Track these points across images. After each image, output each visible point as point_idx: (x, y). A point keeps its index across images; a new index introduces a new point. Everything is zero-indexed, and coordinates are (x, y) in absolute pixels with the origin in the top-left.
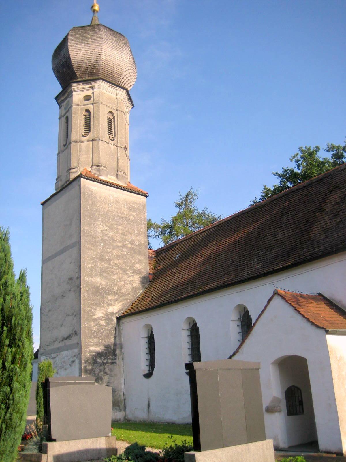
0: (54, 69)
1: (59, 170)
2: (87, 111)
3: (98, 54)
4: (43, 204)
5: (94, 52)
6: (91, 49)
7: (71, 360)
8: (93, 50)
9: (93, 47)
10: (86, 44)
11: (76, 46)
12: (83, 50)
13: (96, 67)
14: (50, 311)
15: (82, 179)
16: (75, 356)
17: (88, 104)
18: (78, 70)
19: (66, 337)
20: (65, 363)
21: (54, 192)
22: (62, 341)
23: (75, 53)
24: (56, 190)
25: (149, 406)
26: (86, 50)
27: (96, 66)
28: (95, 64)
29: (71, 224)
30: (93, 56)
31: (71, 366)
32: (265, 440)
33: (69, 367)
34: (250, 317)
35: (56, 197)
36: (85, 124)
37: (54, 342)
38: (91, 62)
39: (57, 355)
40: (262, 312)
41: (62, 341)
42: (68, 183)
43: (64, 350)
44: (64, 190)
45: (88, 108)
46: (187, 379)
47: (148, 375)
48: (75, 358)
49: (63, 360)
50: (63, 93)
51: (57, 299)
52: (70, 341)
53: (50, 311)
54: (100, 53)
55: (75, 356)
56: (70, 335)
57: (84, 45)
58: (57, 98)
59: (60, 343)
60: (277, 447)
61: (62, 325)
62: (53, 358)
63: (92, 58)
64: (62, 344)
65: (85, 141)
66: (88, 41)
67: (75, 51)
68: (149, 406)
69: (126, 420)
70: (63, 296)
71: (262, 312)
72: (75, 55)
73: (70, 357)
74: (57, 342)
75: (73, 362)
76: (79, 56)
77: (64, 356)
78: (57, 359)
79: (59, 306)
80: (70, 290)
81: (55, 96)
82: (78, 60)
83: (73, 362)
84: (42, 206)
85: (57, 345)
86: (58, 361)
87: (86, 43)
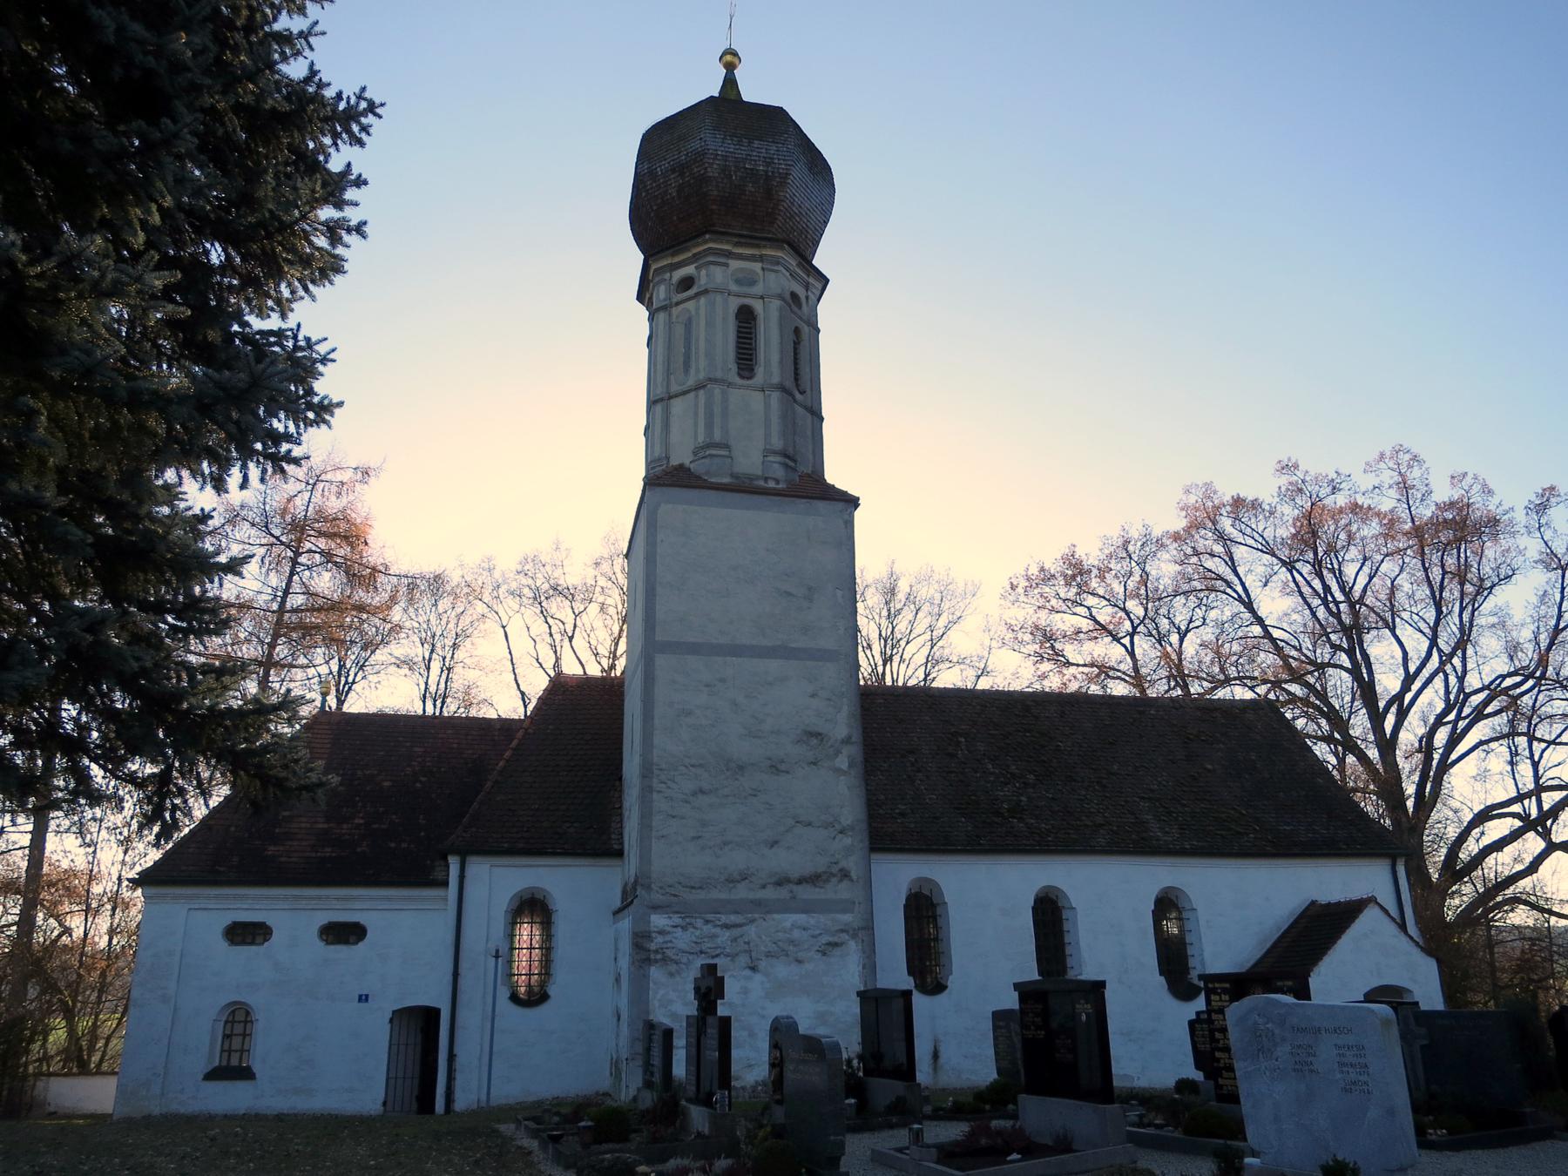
19: (795, 875)
20: (795, 946)
34: (352, 939)
55: (842, 931)
59: (764, 887)
61: (774, 844)
62: (726, 926)
64: (770, 894)
73: (818, 932)
77: (788, 924)
78: (751, 931)
85: (742, 892)
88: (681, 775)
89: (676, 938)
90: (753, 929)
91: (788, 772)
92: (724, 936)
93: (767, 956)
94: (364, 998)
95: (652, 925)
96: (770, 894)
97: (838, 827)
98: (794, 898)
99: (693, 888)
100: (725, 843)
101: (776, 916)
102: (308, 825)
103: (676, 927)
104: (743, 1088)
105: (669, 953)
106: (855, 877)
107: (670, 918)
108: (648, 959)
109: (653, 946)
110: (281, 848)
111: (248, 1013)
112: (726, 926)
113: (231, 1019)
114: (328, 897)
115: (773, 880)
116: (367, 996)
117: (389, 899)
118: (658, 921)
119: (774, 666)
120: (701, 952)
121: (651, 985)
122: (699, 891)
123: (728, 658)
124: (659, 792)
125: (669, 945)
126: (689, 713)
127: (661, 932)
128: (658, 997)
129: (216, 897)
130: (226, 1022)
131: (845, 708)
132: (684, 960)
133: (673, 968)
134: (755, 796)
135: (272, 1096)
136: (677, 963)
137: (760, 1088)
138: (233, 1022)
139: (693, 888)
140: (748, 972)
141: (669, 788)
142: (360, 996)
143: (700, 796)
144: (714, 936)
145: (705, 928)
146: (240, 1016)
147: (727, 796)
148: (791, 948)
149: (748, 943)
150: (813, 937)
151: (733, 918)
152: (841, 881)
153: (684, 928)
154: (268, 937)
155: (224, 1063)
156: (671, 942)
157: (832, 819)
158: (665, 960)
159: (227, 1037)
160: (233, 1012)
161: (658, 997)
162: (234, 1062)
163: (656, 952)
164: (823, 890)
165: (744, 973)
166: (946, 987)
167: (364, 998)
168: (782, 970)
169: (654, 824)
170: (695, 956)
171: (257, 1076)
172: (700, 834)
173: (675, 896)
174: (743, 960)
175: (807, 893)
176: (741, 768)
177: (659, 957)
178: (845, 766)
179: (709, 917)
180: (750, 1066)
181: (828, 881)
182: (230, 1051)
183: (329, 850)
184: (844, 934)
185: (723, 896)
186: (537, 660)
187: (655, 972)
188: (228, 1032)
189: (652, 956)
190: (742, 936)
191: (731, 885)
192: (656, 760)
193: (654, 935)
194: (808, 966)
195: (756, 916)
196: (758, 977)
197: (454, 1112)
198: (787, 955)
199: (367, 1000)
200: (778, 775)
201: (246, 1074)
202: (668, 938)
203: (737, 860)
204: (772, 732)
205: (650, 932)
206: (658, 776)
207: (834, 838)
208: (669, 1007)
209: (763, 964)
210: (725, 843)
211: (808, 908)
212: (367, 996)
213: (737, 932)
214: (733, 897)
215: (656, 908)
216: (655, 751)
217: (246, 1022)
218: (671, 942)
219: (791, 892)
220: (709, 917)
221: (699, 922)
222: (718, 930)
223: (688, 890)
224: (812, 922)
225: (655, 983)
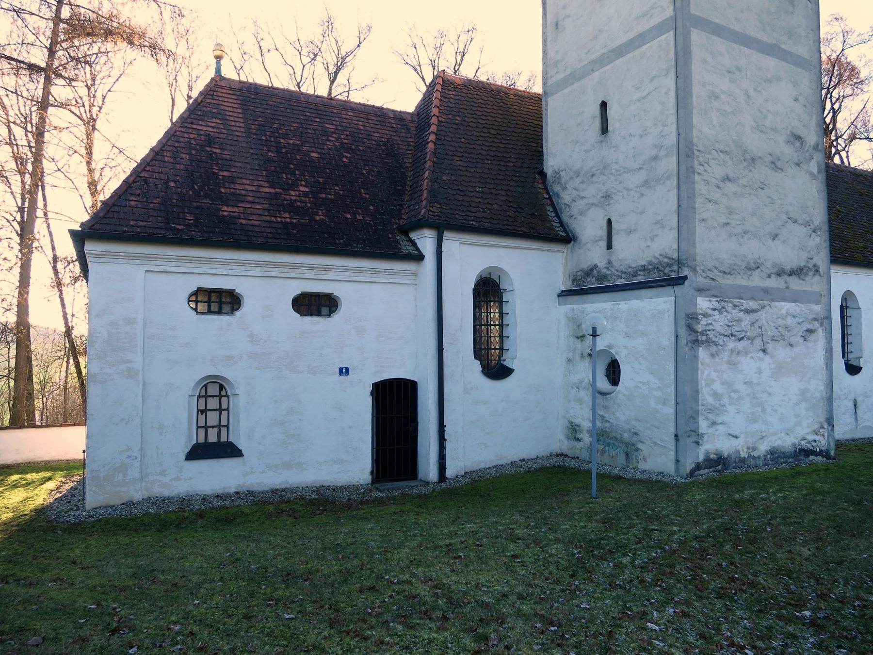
1: (546, 21)
7: (806, 326)
16: (815, 319)
19: (788, 268)
20: (789, 331)
31: (805, 340)
32: (616, 360)
33: (801, 341)
34: (325, 310)
39: (763, 307)
43: (784, 300)
46: (171, 101)
48: (816, 324)
49: (780, 322)
55: (815, 319)
59: (769, 277)
60: (494, 277)
61: (775, 237)
62: (748, 312)
64: (773, 283)
73: (801, 320)
74: (756, 273)
75: (810, 331)
77: (784, 312)
78: (762, 315)
83: (810, 331)
85: (757, 280)
86: (764, 322)
88: (713, 159)
89: (715, 321)
90: (764, 315)
91: (782, 170)
92: (747, 319)
93: (772, 340)
94: (344, 371)
95: (698, 307)
96: (773, 283)
97: (812, 226)
98: (787, 288)
99: (725, 273)
100: (745, 232)
101: (777, 304)
102: (254, 189)
103: (714, 310)
104: (759, 457)
105: (711, 335)
106: (822, 273)
107: (710, 301)
108: (697, 341)
109: (700, 328)
110: (236, 209)
111: (222, 387)
112: (748, 312)
113: (203, 393)
114: (302, 266)
115: (774, 271)
116: (347, 369)
117: (361, 270)
118: (703, 304)
119: (771, 63)
120: (732, 335)
121: (700, 366)
122: (729, 276)
123: (742, 47)
124: (699, 174)
125: (711, 327)
126: (717, 97)
127: (705, 315)
128: (705, 377)
129: (180, 259)
130: (199, 397)
131: (814, 116)
132: (721, 343)
133: (714, 349)
134: (763, 189)
135: (262, 472)
136: (716, 345)
137: (769, 456)
138: (206, 396)
139: (725, 273)
140: (761, 354)
141: (705, 171)
142: (341, 369)
143: (728, 183)
144: (739, 320)
145: (734, 311)
146: (213, 390)
147: (745, 186)
148: (786, 333)
149: (760, 327)
150: (799, 324)
151: (751, 304)
152: (814, 275)
153: (720, 311)
154: (333, 309)
155: (202, 440)
156: (711, 324)
157: (808, 219)
158: (709, 342)
159: (203, 412)
160: (206, 386)
161: (705, 377)
162: (213, 438)
163: (702, 333)
164: (804, 282)
165: (758, 355)
166: (861, 368)
167: (344, 371)
168: (781, 352)
169: (697, 206)
170: (728, 339)
171: (244, 452)
172: (728, 221)
173: (713, 280)
174: (758, 342)
175: (795, 284)
176: (753, 160)
177: (704, 338)
178: (815, 171)
179: (736, 302)
180: (763, 437)
181: (806, 274)
182: (206, 427)
183: (287, 215)
184: (816, 322)
185: (744, 282)
186: (104, 99)
187: (702, 353)
188: (202, 407)
189: (700, 338)
190: (757, 321)
191: (750, 273)
192: (695, 140)
193: (700, 317)
194: (796, 349)
195: (766, 302)
196: (767, 359)
197: (447, 478)
198: (784, 340)
199: (347, 373)
200: (776, 171)
201: (229, 450)
202: (710, 320)
203: (753, 249)
204: (772, 129)
205: (697, 314)
206: (698, 157)
207: (810, 236)
208: (712, 387)
209: (770, 347)
210: (745, 232)
211: (795, 299)
212: (347, 369)
213: (754, 316)
214: (751, 284)
215: (701, 290)
216: (694, 130)
217: (220, 396)
218: (711, 324)
219: (786, 282)
220: (736, 302)
221: (729, 306)
222: (741, 315)
223: (721, 275)
224: (798, 310)
225: (702, 364)
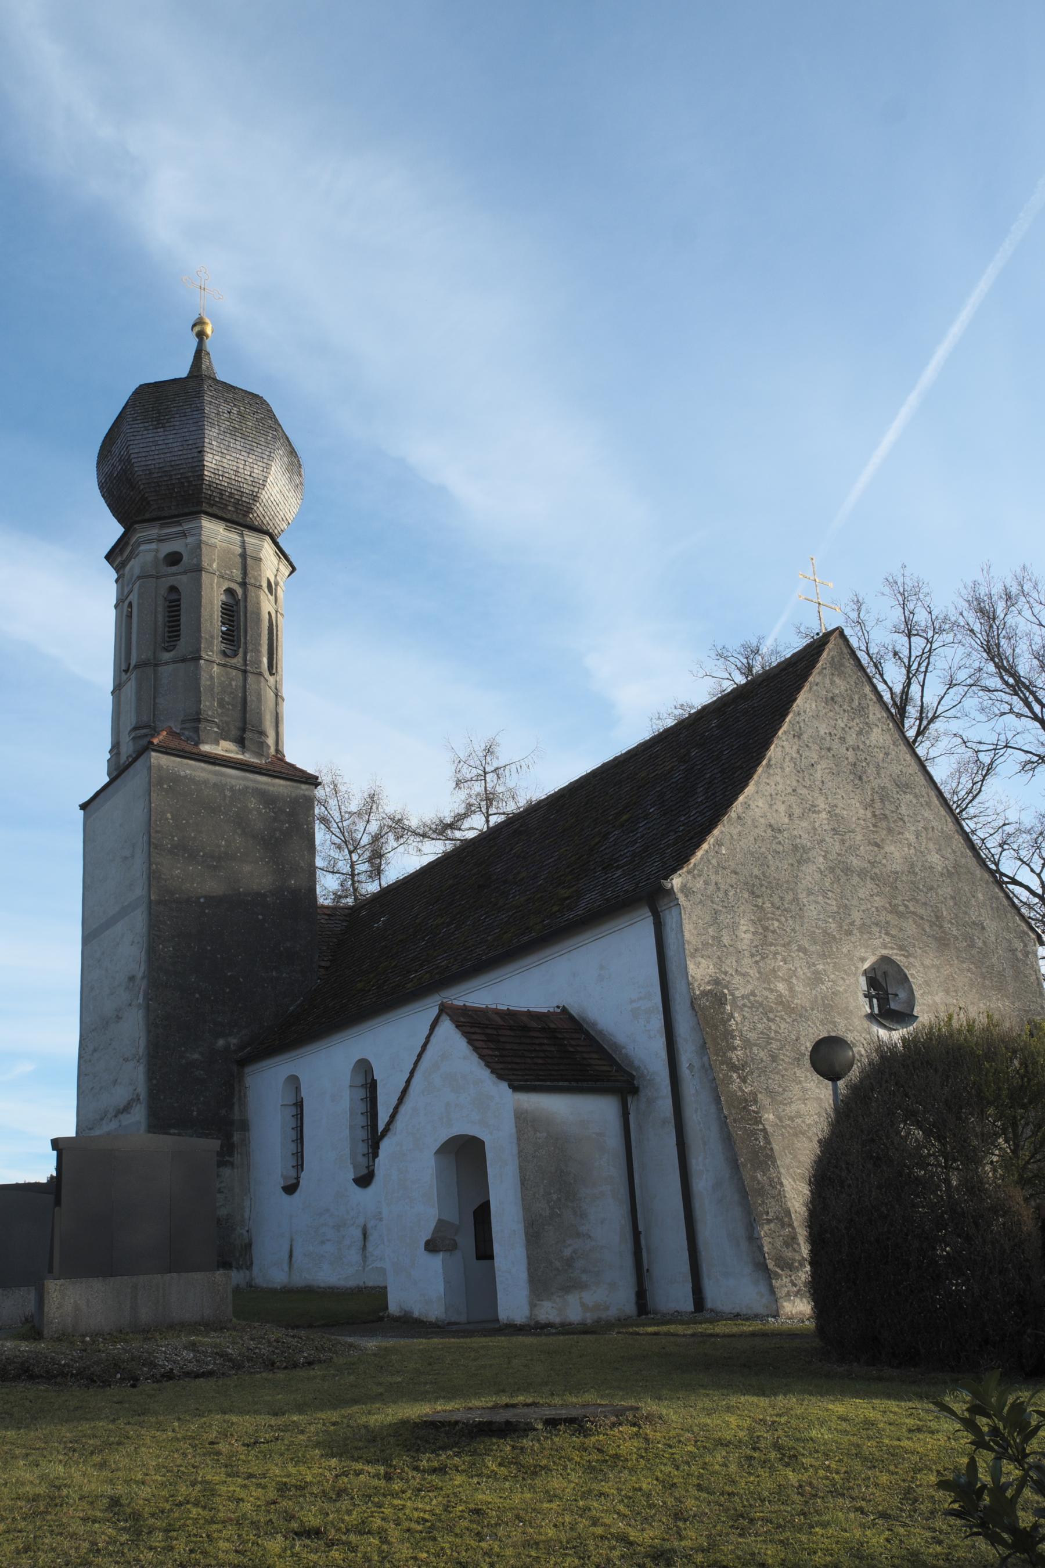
0: (101, 487)
2: (173, 589)
3: (196, 450)
4: (84, 807)
5: (186, 447)
6: (179, 440)
8: (184, 443)
9: (183, 435)
10: (168, 429)
11: (145, 432)
12: (160, 442)
13: (194, 483)
14: (95, 1050)
15: (153, 754)
17: (174, 574)
18: (152, 489)
19: (121, 1107)
21: (107, 779)
22: (116, 1116)
23: (141, 450)
24: (109, 774)
25: (291, 1256)
26: (166, 442)
27: (192, 479)
28: (190, 474)
29: (133, 856)
30: (185, 457)
35: (110, 788)
36: (169, 622)
37: (102, 1119)
38: (181, 471)
40: (420, 1056)
41: (116, 1116)
42: (130, 760)
44: (123, 776)
45: (175, 584)
47: (290, 1189)
50: (120, 546)
51: (107, 1023)
52: (129, 1116)
53: (95, 1050)
54: (199, 449)
56: (129, 1104)
57: (162, 430)
58: (110, 557)
63: (183, 462)
65: (168, 663)
66: (172, 420)
67: (141, 445)
68: (291, 1256)
69: (251, 1286)
70: (119, 1018)
71: (420, 1056)
72: (144, 454)
76: (152, 458)
79: (111, 1039)
80: (130, 1005)
81: (105, 554)
82: (150, 467)
84: (82, 811)
87: (167, 425)
